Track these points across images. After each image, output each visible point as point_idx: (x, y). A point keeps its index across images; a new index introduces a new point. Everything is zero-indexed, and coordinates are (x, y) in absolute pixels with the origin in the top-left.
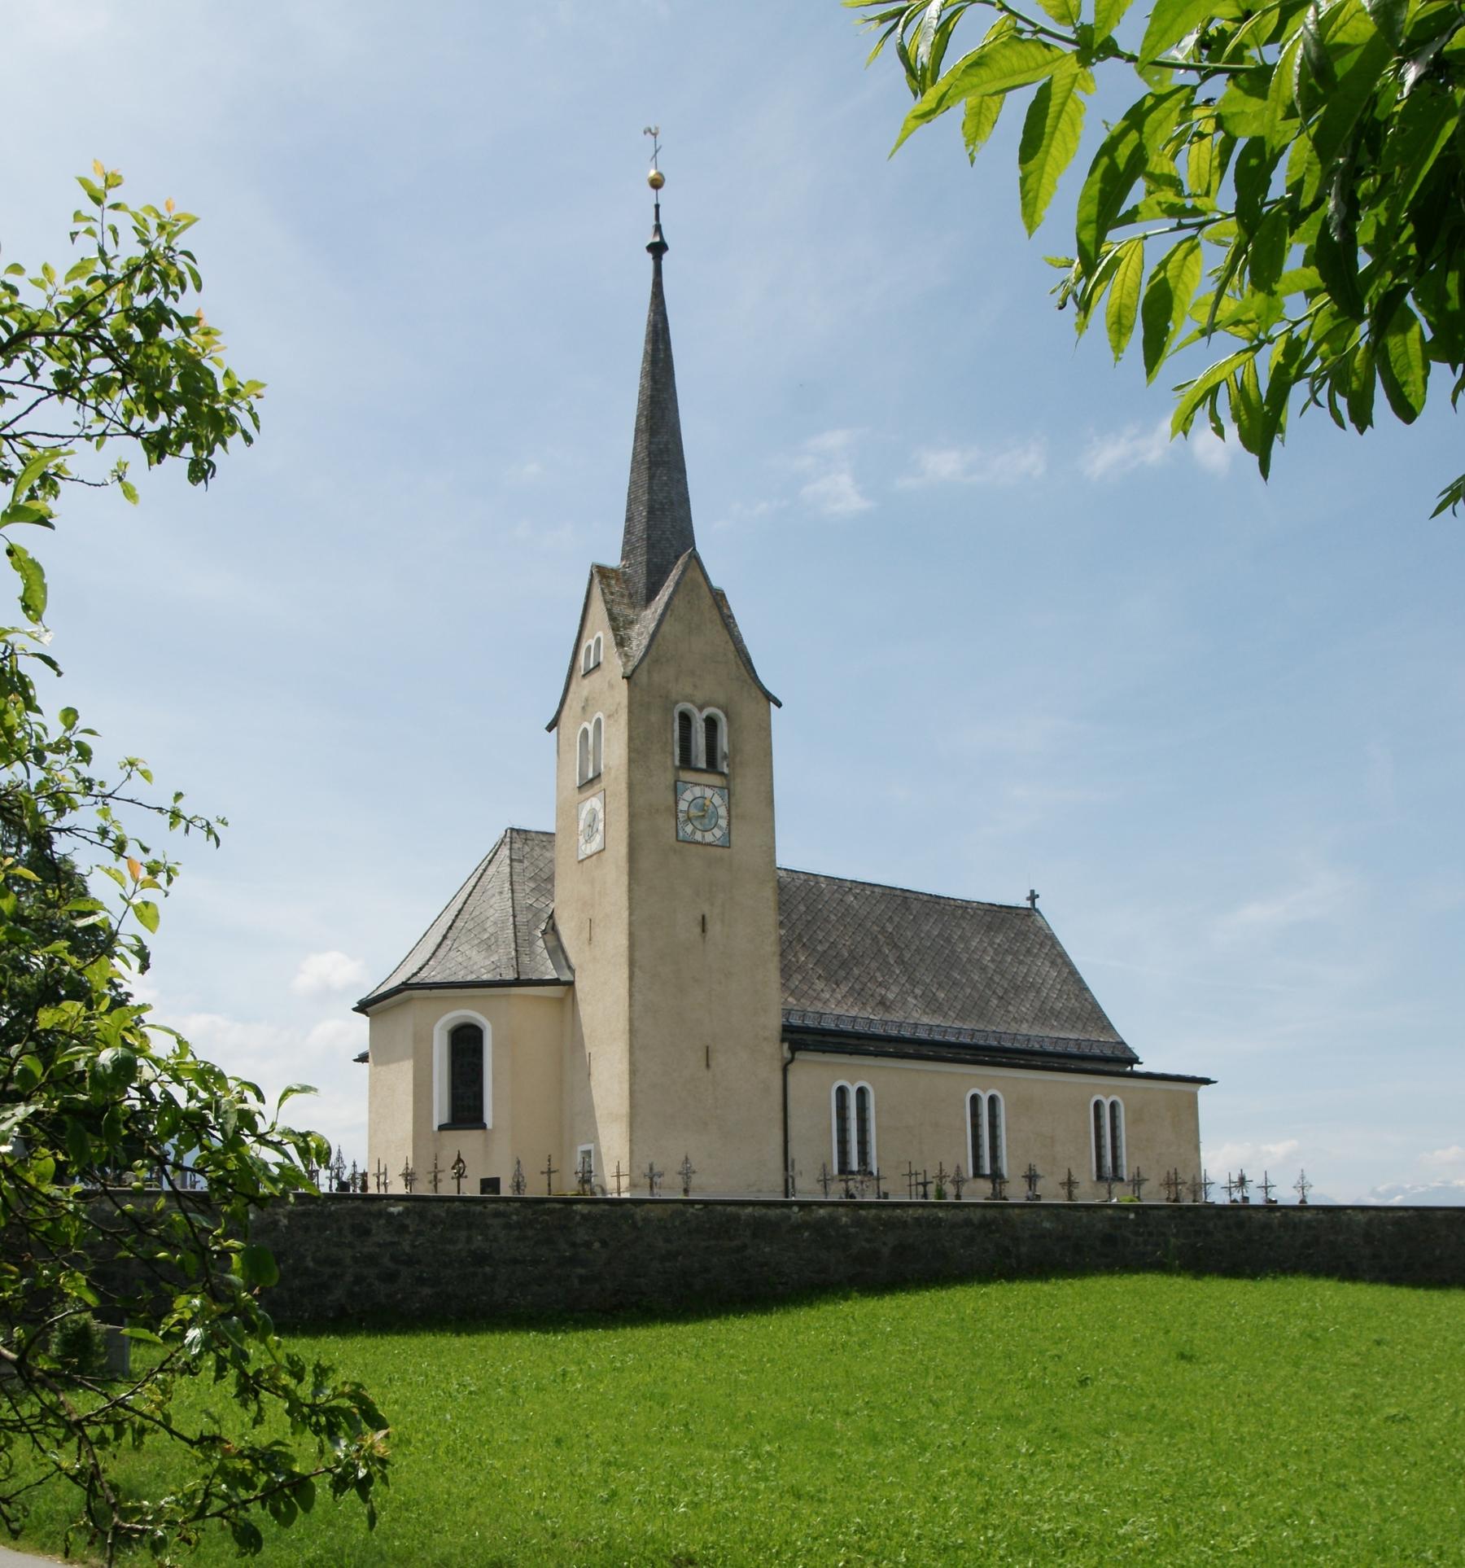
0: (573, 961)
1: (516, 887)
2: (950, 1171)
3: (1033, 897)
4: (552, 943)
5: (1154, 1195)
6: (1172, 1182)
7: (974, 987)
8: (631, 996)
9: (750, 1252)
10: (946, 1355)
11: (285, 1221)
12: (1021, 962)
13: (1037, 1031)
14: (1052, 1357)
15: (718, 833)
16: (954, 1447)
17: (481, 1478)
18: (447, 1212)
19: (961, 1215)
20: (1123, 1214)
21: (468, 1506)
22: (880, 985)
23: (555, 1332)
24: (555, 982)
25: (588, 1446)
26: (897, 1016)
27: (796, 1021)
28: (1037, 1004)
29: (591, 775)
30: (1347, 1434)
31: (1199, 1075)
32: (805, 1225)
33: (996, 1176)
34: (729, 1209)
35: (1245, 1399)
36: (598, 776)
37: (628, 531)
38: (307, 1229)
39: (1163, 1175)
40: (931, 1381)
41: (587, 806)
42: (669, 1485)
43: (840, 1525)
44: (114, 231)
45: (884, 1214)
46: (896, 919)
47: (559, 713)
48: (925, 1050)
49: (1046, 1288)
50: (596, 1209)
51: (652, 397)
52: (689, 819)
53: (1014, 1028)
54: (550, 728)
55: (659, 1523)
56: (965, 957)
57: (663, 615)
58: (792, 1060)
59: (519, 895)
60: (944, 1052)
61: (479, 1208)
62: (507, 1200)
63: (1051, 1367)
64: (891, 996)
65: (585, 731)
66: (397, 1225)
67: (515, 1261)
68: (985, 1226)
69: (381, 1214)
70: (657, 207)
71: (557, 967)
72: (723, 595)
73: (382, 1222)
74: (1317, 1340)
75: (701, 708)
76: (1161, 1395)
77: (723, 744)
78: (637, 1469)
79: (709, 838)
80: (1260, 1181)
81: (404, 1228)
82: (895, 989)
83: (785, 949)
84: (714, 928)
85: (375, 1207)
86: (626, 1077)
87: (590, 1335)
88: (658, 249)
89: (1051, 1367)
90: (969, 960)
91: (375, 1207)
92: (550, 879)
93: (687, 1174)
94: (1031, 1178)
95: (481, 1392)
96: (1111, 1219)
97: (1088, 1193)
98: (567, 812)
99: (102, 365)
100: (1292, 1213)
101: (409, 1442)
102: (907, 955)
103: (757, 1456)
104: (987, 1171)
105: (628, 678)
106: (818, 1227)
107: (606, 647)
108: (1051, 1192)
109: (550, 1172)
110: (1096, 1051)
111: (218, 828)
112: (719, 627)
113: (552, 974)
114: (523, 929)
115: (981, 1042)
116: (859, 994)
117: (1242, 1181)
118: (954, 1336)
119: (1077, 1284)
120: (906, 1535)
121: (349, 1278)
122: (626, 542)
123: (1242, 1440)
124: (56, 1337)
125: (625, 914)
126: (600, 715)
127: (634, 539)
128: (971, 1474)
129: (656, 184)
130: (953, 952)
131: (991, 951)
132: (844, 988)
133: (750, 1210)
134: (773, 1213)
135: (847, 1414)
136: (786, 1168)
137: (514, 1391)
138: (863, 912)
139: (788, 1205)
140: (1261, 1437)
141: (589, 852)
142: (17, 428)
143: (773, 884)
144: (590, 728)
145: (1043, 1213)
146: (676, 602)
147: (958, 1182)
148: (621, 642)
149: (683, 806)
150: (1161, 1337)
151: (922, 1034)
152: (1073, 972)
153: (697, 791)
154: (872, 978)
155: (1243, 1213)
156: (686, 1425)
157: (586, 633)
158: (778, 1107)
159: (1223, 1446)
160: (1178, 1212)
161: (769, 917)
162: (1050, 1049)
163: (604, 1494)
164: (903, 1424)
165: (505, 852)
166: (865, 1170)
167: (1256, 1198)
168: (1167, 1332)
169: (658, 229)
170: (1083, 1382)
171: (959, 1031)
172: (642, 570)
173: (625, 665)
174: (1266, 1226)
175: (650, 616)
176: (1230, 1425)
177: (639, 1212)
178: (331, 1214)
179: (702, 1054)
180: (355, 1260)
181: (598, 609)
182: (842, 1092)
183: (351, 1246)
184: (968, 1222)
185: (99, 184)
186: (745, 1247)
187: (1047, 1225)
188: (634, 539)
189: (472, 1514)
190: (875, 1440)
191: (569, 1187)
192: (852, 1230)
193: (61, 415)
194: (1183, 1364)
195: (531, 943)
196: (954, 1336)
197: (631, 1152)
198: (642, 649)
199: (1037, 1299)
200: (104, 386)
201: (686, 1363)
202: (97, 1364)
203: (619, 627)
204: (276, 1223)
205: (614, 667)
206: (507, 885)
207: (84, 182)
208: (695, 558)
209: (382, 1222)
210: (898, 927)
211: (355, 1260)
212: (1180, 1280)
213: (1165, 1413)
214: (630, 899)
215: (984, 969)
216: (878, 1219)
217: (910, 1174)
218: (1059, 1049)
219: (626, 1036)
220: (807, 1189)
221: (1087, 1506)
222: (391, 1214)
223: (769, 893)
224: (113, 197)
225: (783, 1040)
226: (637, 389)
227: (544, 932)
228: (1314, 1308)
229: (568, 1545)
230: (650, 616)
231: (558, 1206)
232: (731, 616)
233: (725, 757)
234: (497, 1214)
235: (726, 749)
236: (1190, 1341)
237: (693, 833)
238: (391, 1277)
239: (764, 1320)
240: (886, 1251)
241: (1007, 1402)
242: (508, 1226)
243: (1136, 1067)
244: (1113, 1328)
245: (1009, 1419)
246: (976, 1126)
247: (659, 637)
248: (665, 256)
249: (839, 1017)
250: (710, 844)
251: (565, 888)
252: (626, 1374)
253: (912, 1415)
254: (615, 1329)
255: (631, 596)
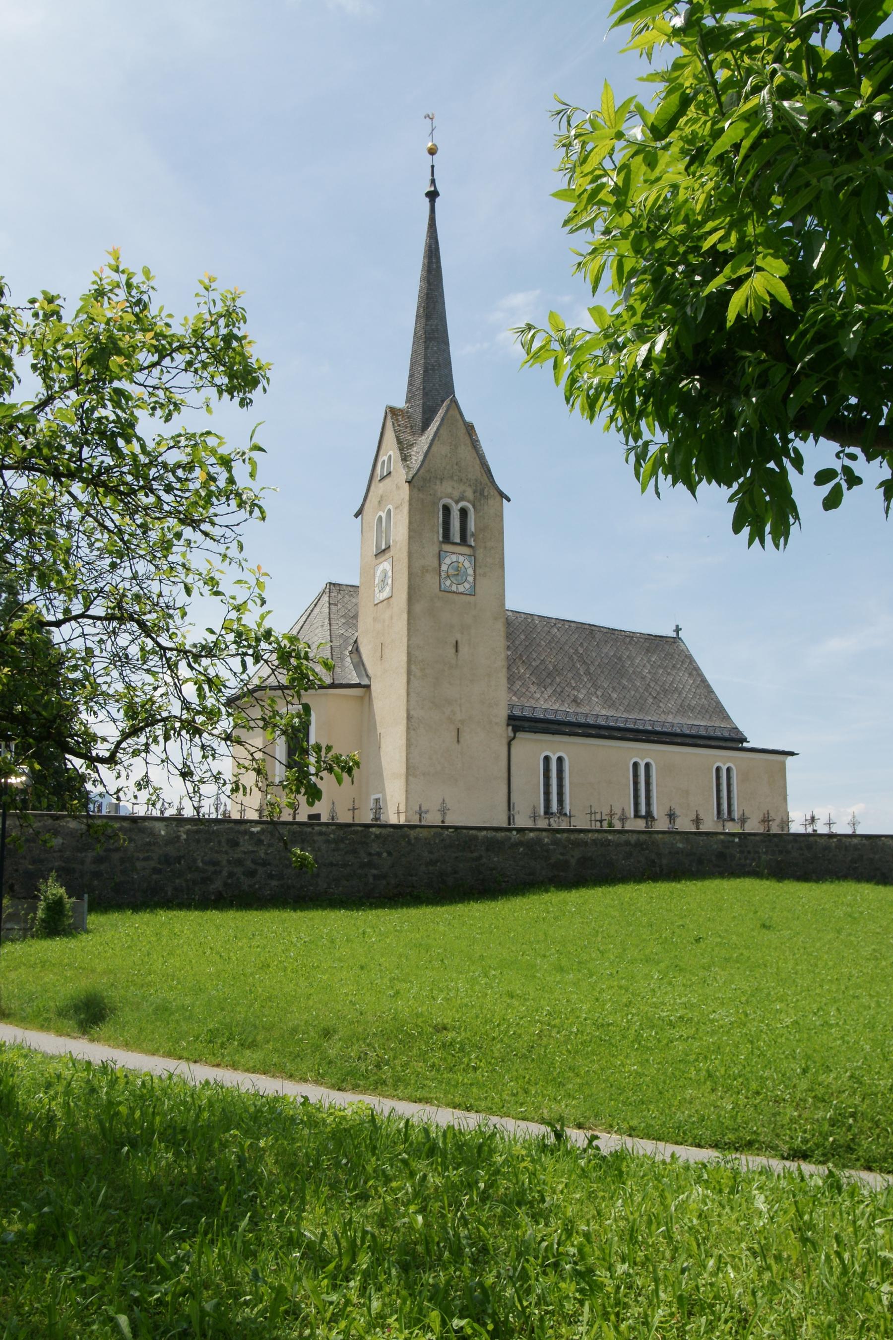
0: (370, 672)
1: (333, 622)
2: (618, 811)
3: (678, 630)
4: (356, 660)
5: (753, 826)
6: (766, 820)
7: (637, 691)
8: (408, 694)
9: (484, 860)
10: (610, 924)
11: (184, 836)
12: (669, 674)
13: (678, 720)
14: (679, 927)
15: (467, 585)
16: (611, 974)
17: (315, 984)
18: (289, 831)
19: (624, 838)
20: (731, 839)
21: (308, 999)
22: (574, 688)
23: (358, 910)
24: (358, 686)
25: (381, 971)
26: (584, 710)
27: (517, 713)
28: (679, 702)
29: (383, 547)
30: (865, 971)
31: (787, 750)
32: (520, 843)
33: (649, 816)
34: (471, 832)
35: (802, 951)
36: (388, 548)
37: (410, 384)
38: (198, 841)
39: (761, 816)
40: (599, 939)
41: (380, 568)
42: (431, 990)
43: (537, 1011)
44: (214, 301)
45: (572, 837)
46: (585, 645)
47: (363, 505)
48: (603, 732)
49: (679, 886)
50: (384, 831)
51: (427, 294)
52: (448, 576)
53: (663, 718)
54: (357, 516)
55: (425, 1008)
56: (631, 670)
57: (433, 440)
58: (514, 738)
59: (334, 627)
60: (616, 734)
61: (309, 829)
62: (327, 824)
63: (677, 931)
64: (581, 696)
65: (380, 518)
66: (256, 839)
67: (331, 864)
68: (639, 845)
69: (246, 832)
70: (433, 167)
71: (359, 676)
72: (472, 427)
73: (247, 837)
74: (855, 918)
75: (457, 502)
76: (747, 948)
77: (472, 526)
78: (411, 982)
79: (461, 589)
80: (826, 820)
81: (260, 842)
82: (584, 691)
83: (511, 664)
84: (464, 650)
85: (242, 828)
86: (404, 748)
87: (379, 912)
88: (433, 195)
89: (677, 931)
90: (634, 672)
91: (242, 828)
92: (355, 617)
93: (443, 811)
94: (671, 816)
95: (311, 942)
96: (723, 842)
97: (709, 824)
98: (367, 572)
99: (204, 356)
100: (844, 839)
101: (269, 966)
102: (592, 669)
103: (486, 976)
104: (643, 812)
105: (409, 482)
106: (530, 846)
107: (395, 462)
108: (684, 824)
109: (354, 809)
110: (718, 734)
111: (243, 563)
112: (470, 448)
113: (355, 680)
114: (337, 650)
115: (641, 727)
116: (559, 695)
117: (813, 819)
118: (616, 914)
119: (699, 884)
120: (578, 1017)
121: (225, 873)
122: (409, 392)
123: (796, 973)
124: (42, 905)
125: (405, 639)
126: (390, 507)
127: (414, 389)
128: (620, 987)
129: (432, 152)
130: (623, 667)
131: (649, 666)
132: (550, 691)
133: (484, 833)
134: (500, 835)
135: (545, 956)
136: (509, 810)
137: (332, 942)
138: (563, 640)
139: (509, 830)
140: (809, 971)
141: (381, 599)
142: (167, 386)
143: (503, 620)
144: (384, 515)
145: (678, 837)
146: (441, 431)
147: (623, 819)
148: (405, 458)
149: (444, 567)
150: (751, 915)
151: (601, 722)
152: (704, 681)
153: (454, 558)
154: (569, 684)
155: (811, 839)
156: (442, 961)
157: (381, 453)
158: (505, 770)
159: (783, 975)
160: (768, 838)
161: (500, 642)
162: (688, 732)
163: (391, 992)
164: (579, 963)
165: (325, 598)
166: (561, 812)
167: (822, 829)
168: (756, 912)
169: (433, 182)
170: (698, 940)
171: (626, 720)
172: (419, 410)
173: (407, 473)
174: (826, 848)
175: (424, 440)
176: (790, 965)
177: (413, 833)
178: (214, 832)
179: (455, 734)
180: (229, 862)
181: (390, 435)
182: (547, 759)
183: (226, 853)
184: (628, 843)
185: (207, 281)
186: (480, 857)
187: (680, 845)
188: (414, 389)
189: (311, 1003)
190: (561, 970)
191: (367, 818)
192: (551, 847)
193: (188, 378)
194: (764, 931)
195: (342, 660)
196: (616, 914)
197: (407, 799)
198: (419, 463)
199: (672, 893)
200: (205, 366)
201: (441, 928)
202: (67, 923)
203: (404, 448)
204: (178, 837)
205: (401, 475)
206: (327, 621)
207: (201, 282)
208: (455, 402)
209: (247, 837)
210: (586, 649)
211: (229, 862)
212: (768, 883)
213: (749, 958)
214: (409, 630)
215: (643, 678)
216: (568, 840)
217: (591, 813)
218: (693, 732)
219: (405, 721)
220: (521, 821)
221: (692, 1005)
222: (252, 833)
223: (500, 626)
224: (214, 285)
225: (508, 725)
226: (418, 288)
227: (351, 652)
228: (855, 900)
229: (370, 1018)
230: (424, 440)
231: (360, 829)
232: (478, 441)
233: (473, 535)
234: (321, 833)
235: (473, 529)
236: (771, 918)
237: (451, 586)
238: (251, 874)
239: (493, 904)
240: (573, 862)
241: (647, 951)
242: (328, 841)
243: (745, 745)
244: (720, 910)
245: (647, 960)
246: (636, 783)
247: (430, 455)
248: (437, 200)
249: (546, 710)
250: (461, 593)
251: (365, 622)
252: (404, 934)
253: (585, 957)
254: (396, 909)
255: (412, 427)
